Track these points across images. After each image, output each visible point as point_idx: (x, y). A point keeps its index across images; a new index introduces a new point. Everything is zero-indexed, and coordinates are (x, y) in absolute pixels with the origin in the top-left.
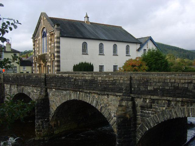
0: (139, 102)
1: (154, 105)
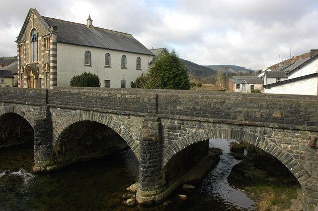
0: (166, 123)
1: (183, 127)
